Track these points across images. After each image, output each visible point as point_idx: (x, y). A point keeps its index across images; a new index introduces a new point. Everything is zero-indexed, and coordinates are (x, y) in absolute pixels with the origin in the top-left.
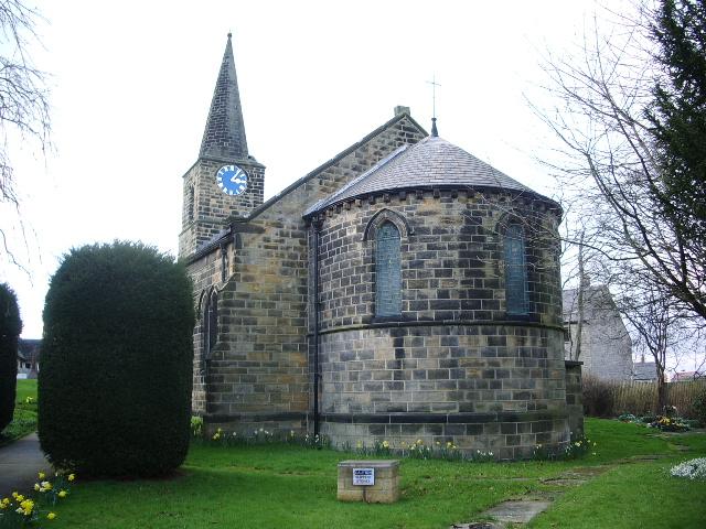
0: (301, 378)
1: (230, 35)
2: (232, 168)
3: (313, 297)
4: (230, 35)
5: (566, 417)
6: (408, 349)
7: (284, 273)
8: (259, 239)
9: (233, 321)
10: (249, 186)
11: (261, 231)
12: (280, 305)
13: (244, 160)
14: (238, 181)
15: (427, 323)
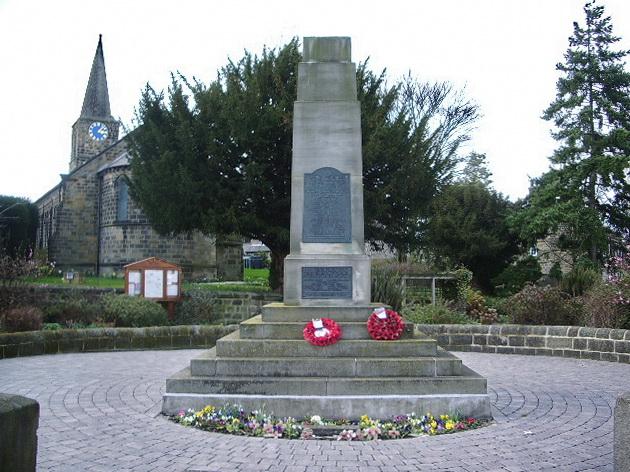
0: (94, 248)
1: (101, 36)
2: (99, 124)
3: (98, 212)
4: (101, 36)
5: (536, 215)
6: (128, 235)
7: (87, 199)
8: (75, 184)
9: (62, 222)
10: (109, 134)
11: (76, 180)
12: (84, 214)
13: (107, 119)
14: (102, 132)
15: (135, 224)
